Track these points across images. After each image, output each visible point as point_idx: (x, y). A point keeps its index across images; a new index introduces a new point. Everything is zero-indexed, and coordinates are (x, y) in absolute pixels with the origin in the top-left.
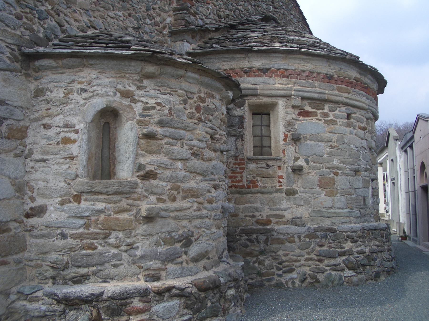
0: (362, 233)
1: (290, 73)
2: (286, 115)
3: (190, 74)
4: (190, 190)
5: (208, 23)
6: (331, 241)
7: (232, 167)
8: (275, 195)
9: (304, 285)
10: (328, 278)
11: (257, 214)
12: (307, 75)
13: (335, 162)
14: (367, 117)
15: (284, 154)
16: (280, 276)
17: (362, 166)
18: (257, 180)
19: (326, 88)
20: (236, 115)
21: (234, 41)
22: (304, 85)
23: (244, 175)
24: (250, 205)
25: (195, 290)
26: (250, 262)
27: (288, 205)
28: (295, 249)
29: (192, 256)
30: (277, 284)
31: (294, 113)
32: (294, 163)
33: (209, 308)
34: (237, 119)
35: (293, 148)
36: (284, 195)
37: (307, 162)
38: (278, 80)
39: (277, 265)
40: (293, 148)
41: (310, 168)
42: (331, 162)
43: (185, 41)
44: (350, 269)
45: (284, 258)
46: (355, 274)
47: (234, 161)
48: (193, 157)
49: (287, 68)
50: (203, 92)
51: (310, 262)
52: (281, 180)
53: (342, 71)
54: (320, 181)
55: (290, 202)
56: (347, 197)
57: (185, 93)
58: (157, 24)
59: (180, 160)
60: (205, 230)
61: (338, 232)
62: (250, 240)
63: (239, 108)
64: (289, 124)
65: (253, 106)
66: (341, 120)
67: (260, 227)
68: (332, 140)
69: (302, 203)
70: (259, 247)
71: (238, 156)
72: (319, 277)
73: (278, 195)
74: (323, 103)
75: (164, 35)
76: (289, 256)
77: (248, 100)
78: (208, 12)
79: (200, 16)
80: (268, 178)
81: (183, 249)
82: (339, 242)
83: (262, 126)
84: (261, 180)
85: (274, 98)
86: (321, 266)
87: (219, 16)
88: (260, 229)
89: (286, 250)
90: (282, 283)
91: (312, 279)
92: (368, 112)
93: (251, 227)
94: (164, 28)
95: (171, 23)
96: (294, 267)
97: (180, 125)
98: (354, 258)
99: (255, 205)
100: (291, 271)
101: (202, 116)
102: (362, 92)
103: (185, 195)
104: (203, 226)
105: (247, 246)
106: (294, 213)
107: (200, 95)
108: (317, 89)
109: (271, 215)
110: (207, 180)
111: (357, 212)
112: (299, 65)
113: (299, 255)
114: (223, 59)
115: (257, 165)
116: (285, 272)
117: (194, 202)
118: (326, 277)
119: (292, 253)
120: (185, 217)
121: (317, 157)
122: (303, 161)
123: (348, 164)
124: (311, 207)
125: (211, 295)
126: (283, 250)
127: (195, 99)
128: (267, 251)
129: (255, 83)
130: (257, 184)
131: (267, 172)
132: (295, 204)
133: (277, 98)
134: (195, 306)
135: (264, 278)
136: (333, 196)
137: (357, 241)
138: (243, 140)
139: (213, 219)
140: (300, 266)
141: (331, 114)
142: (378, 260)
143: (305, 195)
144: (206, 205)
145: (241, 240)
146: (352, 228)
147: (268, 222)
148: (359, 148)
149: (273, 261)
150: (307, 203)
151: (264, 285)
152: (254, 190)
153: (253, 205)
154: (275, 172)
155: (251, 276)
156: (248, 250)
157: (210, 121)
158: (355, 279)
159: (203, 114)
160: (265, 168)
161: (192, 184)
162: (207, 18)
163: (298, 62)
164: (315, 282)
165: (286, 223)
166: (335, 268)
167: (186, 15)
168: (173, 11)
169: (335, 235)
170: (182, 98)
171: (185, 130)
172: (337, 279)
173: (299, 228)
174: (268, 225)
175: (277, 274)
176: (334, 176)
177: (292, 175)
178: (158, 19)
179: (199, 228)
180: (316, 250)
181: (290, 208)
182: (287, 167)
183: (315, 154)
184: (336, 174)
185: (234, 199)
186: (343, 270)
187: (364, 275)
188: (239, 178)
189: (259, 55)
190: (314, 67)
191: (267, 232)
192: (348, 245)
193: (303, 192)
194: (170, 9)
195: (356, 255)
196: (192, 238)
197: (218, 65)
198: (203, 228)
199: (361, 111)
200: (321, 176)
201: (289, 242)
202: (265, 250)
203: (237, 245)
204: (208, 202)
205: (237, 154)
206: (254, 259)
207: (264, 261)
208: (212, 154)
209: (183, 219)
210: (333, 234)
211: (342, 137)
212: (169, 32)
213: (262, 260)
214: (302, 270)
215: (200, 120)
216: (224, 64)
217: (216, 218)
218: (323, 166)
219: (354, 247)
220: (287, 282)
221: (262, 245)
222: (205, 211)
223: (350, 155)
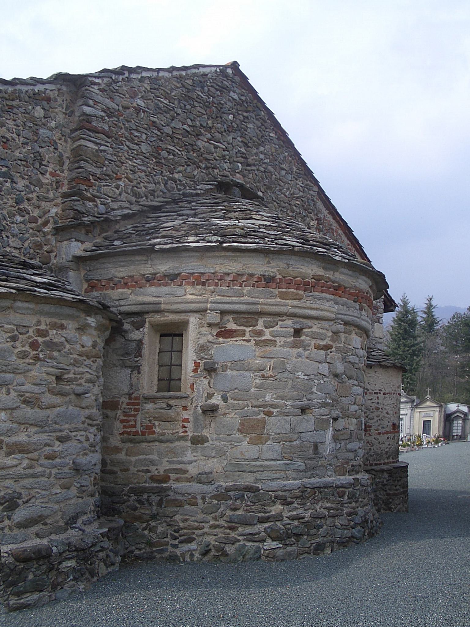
0: (302, 492)
1: (207, 279)
2: (198, 336)
3: (19, 304)
4: (16, 444)
5: (116, 207)
6: (249, 503)
7: (125, 408)
8: (177, 443)
9: (206, 559)
10: (240, 551)
11: (152, 468)
12: (232, 279)
13: (268, 398)
14: (334, 330)
15: (193, 389)
16: (175, 546)
17: (316, 400)
18: (154, 425)
19: (260, 296)
20: (133, 339)
21: (143, 235)
22: (225, 294)
23: (139, 418)
24: (144, 456)
25: (11, 560)
26: (138, 529)
27: (194, 456)
28: (197, 513)
29: (17, 521)
30: (170, 556)
31: (210, 333)
32: (206, 401)
33: (31, 581)
34: (134, 345)
35: (206, 382)
36: (189, 443)
37: (225, 399)
38: (189, 289)
39: (172, 533)
40: (206, 382)
41: (227, 407)
42: (261, 398)
43: (74, 240)
44: (273, 540)
45: (181, 525)
46: (281, 546)
47: (127, 401)
48: (24, 405)
49: (202, 271)
50: (43, 323)
51: (217, 530)
52: (186, 425)
53: (291, 269)
54: (242, 424)
55: (197, 452)
56: (283, 444)
57: (15, 328)
58: (33, 220)
59: (5, 409)
60: (40, 491)
61: (261, 491)
62: (140, 502)
63: (138, 329)
64: (202, 348)
65: (157, 325)
66: (283, 339)
67: (155, 485)
68: (266, 367)
69: (213, 454)
70: (151, 509)
71: (133, 393)
72: (228, 549)
73: (182, 443)
74: (256, 317)
75: (45, 235)
76: (189, 522)
77: (149, 319)
78: (118, 192)
79: (102, 200)
80: (168, 422)
81: (5, 513)
82: (262, 505)
83: (171, 351)
84: (159, 425)
85: (183, 314)
86: (233, 534)
87: (135, 194)
88: (153, 488)
89: (186, 515)
90: (176, 556)
91: (217, 551)
92: (336, 323)
93: (144, 484)
94: (45, 224)
95: (56, 215)
96: (194, 536)
97: (5, 368)
98: (283, 525)
99: (151, 457)
100: (190, 540)
101: (41, 355)
102: (324, 295)
103: (9, 450)
104: (37, 486)
105: (136, 509)
106: (201, 467)
107: (38, 327)
108: (246, 299)
109: (170, 469)
110: (46, 432)
111: (300, 463)
112: (222, 266)
113: (202, 521)
114: (119, 263)
115: (155, 406)
116: (181, 542)
117: (22, 458)
118: (237, 550)
119: (193, 518)
120: (8, 476)
121: (240, 392)
122: (220, 398)
123: (290, 399)
124: (227, 459)
125: (35, 566)
126: (181, 515)
127: (31, 333)
128: (160, 515)
129: (158, 295)
130: (154, 429)
131: (167, 415)
132: (203, 456)
133: (187, 314)
134: (10, 579)
135: (154, 549)
136: (262, 443)
137: (292, 503)
138: (139, 373)
139: (55, 477)
140: (203, 535)
141: (267, 331)
142: (325, 527)
143: (218, 444)
144: (43, 461)
145: (129, 501)
146: (285, 486)
147: (166, 479)
148: (312, 377)
149: (168, 527)
150: (221, 453)
151: (155, 557)
152: (150, 437)
153: (147, 457)
154: (178, 414)
155: (138, 546)
156: (137, 513)
157: (55, 358)
158: (280, 553)
159: (41, 351)
160: (164, 409)
161: (22, 438)
162: (115, 200)
163: (220, 261)
164: (221, 555)
165: (188, 480)
166: (251, 537)
167: (76, 203)
168: (61, 197)
169: (255, 496)
170: (9, 335)
171: (13, 373)
172: (253, 551)
173: (205, 486)
174: (166, 482)
175: (171, 544)
176: (264, 416)
177: (201, 418)
178: (36, 213)
179: (30, 489)
180: (227, 514)
181: (196, 461)
182: (195, 407)
183: (236, 388)
184: (269, 414)
185: (125, 450)
186: (263, 541)
187: (296, 548)
188: (132, 423)
189: (165, 256)
190: (244, 267)
191: (161, 491)
192: (276, 509)
193: (216, 440)
194: (57, 194)
195: (286, 521)
196: (18, 501)
197: (113, 271)
198: (36, 488)
199: (323, 322)
200: (245, 418)
201: (189, 504)
202: (158, 514)
203: (124, 507)
204: (46, 458)
205: (131, 391)
206: (144, 525)
207: (157, 527)
208: (58, 400)
209: (6, 479)
210: (252, 494)
211: (283, 363)
212: (53, 228)
213: (153, 526)
214: (204, 540)
215: (37, 358)
216: (121, 270)
217: (60, 476)
218: (247, 404)
219: (286, 511)
220: (183, 555)
221: (154, 508)
222: (40, 469)
223: (293, 387)
